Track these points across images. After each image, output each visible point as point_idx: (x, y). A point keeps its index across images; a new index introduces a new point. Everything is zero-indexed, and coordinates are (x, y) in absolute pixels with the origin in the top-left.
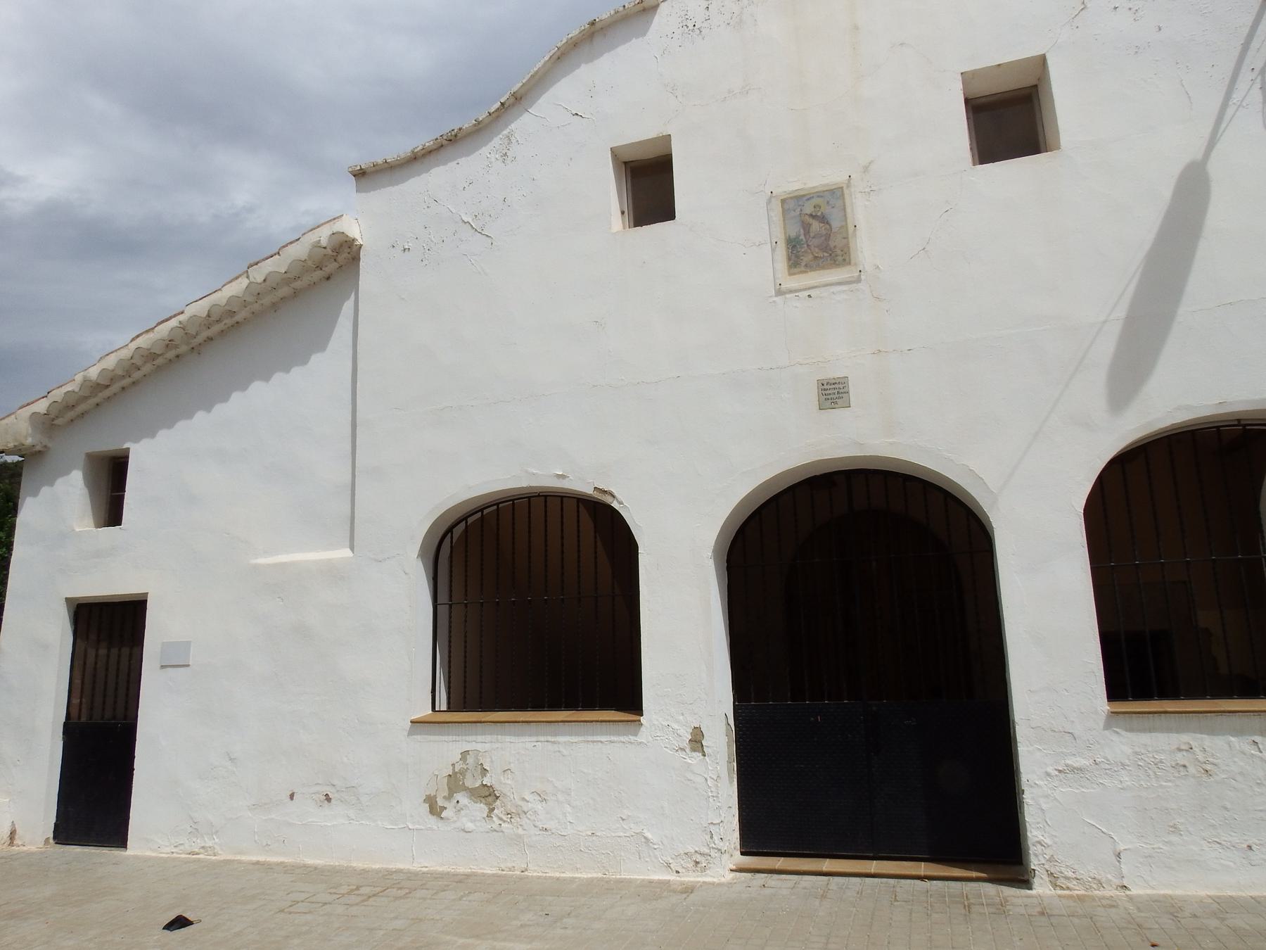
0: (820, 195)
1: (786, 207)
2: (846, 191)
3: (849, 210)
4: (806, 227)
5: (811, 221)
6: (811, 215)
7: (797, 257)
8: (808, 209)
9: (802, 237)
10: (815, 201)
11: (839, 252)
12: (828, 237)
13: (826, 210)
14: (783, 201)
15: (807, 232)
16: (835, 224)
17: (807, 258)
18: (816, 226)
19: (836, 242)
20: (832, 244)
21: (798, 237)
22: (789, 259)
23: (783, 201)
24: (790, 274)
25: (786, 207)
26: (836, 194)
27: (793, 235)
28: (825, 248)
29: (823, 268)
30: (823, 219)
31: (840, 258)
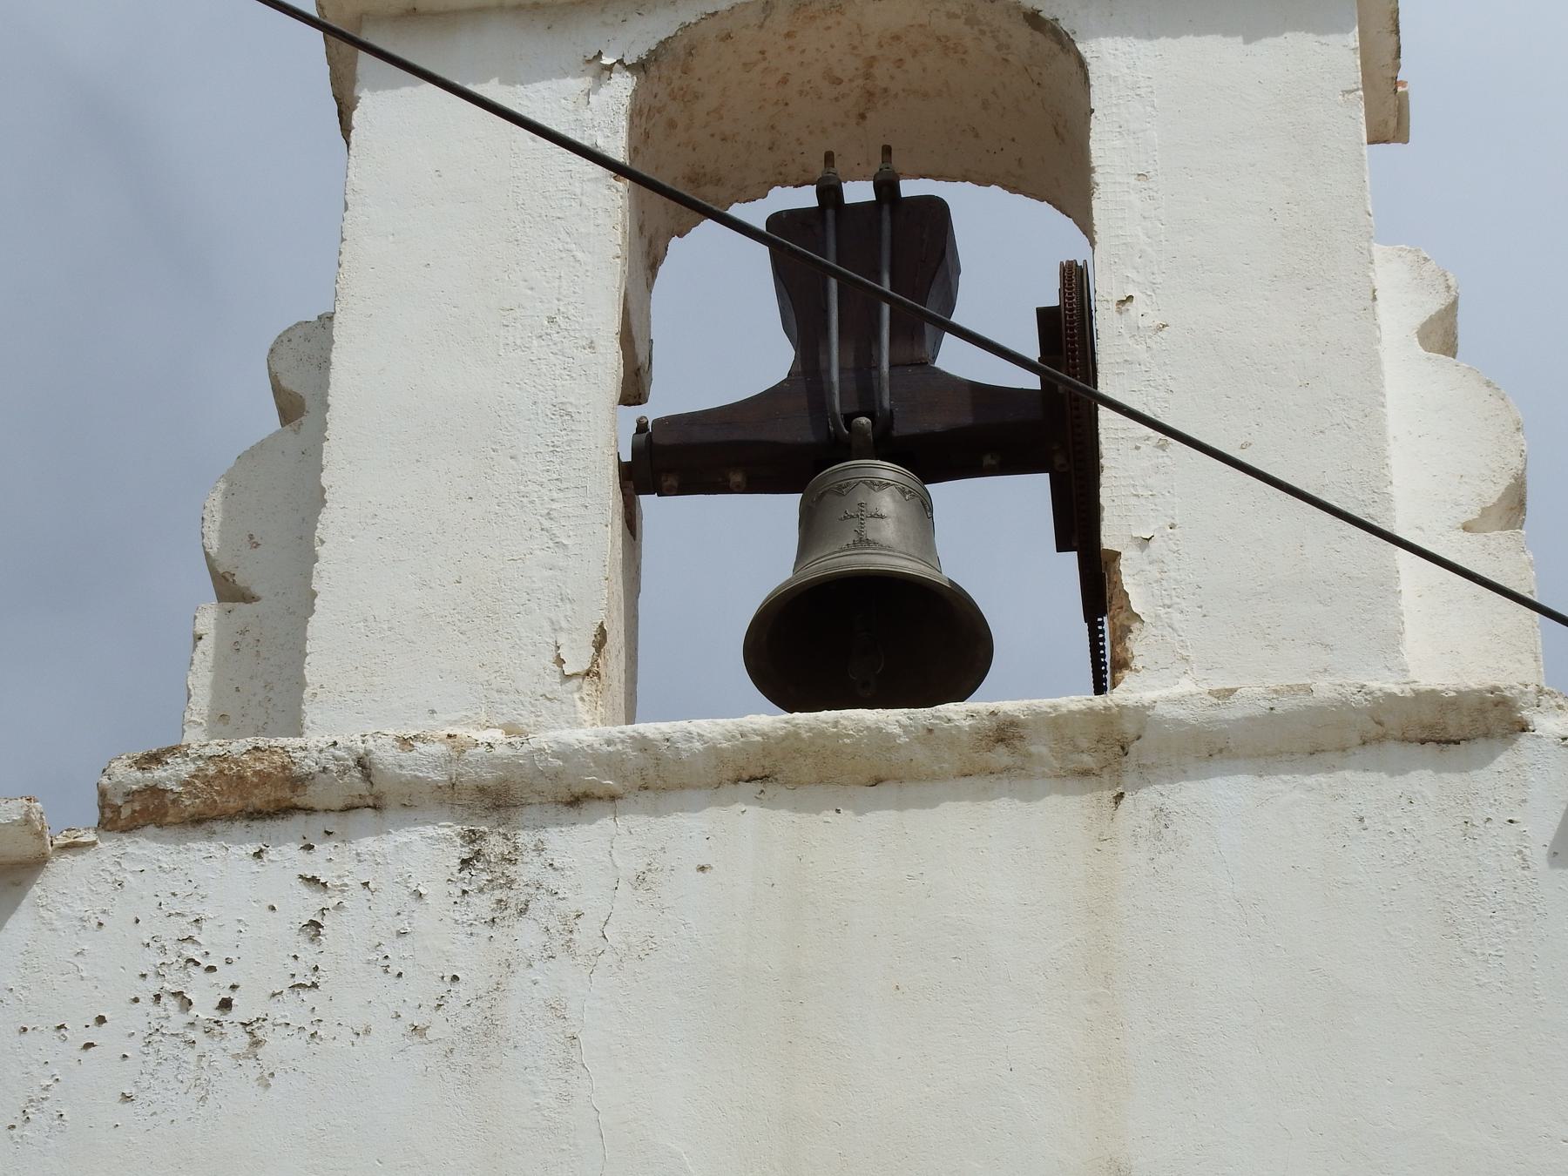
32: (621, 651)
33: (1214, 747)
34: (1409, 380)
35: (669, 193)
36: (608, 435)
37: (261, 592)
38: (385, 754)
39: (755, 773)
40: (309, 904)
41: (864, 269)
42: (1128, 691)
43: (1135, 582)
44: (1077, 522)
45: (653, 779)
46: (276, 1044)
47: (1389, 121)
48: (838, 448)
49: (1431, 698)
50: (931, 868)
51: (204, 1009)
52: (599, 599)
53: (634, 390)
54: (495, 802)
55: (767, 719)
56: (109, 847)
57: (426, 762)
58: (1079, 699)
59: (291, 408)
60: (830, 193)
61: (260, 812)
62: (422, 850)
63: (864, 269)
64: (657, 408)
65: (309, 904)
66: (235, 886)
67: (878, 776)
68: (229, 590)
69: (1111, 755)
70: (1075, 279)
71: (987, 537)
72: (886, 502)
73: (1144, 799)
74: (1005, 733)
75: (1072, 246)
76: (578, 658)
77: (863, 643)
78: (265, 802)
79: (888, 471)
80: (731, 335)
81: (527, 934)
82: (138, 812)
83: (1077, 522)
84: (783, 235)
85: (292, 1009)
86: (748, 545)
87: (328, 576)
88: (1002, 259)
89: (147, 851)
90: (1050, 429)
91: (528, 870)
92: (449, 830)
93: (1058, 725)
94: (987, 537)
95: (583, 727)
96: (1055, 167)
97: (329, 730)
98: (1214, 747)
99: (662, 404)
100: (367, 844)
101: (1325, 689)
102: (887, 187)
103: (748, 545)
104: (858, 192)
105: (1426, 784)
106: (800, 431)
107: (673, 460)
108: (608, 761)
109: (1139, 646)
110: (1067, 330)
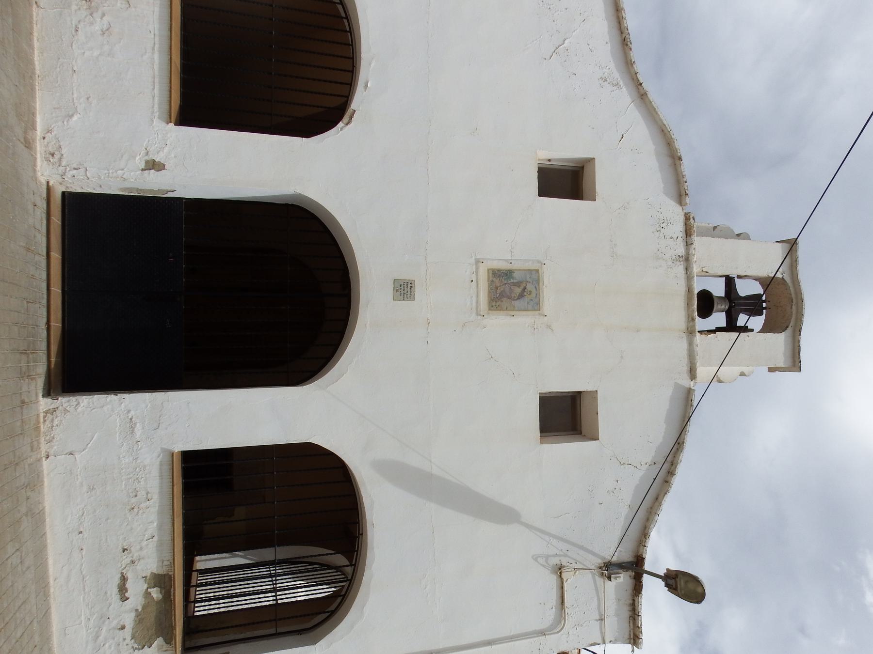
0: (538, 295)
1: (534, 273)
2: (537, 312)
3: (524, 313)
4: (518, 284)
5: (522, 287)
6: (525, 288)
7: (499, 276)
8: (530, 287)
9: (512, 281)
10: (534, 291)
11: (498, 303)
12: (509, 298)
13: (527, 298)
14: (537, 271)
15: (515, 284)
16: (517, 303)
17: (497, 282)
18: (518, 290)
19: (505, 302)
20: (504, 299)
21: (513, 278)
22: (498, 270)
23: (537, 271)
24: (488, 270)
25: (534, 273)
26: (536, 306)
27: (515, 275)
28: (503, 295)
29: (489, 292)
30: (521, 296)
31: (494, 304)
32: (705, 274)
33: (691, 344)
34: (737, 370)
35: (768, 283)
36: (733, 274)
37: (715, 231)
38: (693, 246)
39: (689, 290)
40: (675, 237)
41: (753, 306)
42: (698, 334)
43: (712, 335)
44: (719, 329)
45: (689, 278)
46: (658, 233)
47: (771, 370)
48: (730, 301)
49: (696, 370)
50: (677, 310)
51: (662, 225)
52: (712, 271)
53: (739, 277)
54: (687, 259)
55: (696, 292)
56: (683, 214)
57: (692, 251)
58: (698, 328)
59: (738, 235)
60: (764, 301)
61: (97, 632)
62: (681, 251)
63: (753, 306)
64: (736, 279)
65: (675, 237)
66: (678, 228)
67: (689, 304)
68: (715, 228)
69: (690, 332)
70: (752, 330)
71: (718, 319)
72: (723, 307)
73: (684, 335)
74: (693, 320)
75: (755, 331)
76: (704, 269)
77: (705, 303)
78: (688, 232)
79: (727, 307)
80: (745, 289)
81: (670, 263)
82: (687, 217)
83: (719, 329)
84: (760, 296)
85: (662, 235)
86: (718, 289)
87: (716, 239)
88: (757, 322)
89: (682, 218)
90: (731, 326)
91: (678, 263)
92: (683, 254)
93: (694, 326)
94: (718, 319)
95: (696, 269)
96: (765, 329)
97: (696, 239)
98: (691, 344)
99: (737, 281)
100: (52, 590)
101: (697, 357)
102: (765, 308)
103: (718, 289)
104: (764, 305)
105: (685, 368)
106: (733, 296)
107: (730, 282)
108: (691, 273)
109: (703, 336)
110: (745, 329)
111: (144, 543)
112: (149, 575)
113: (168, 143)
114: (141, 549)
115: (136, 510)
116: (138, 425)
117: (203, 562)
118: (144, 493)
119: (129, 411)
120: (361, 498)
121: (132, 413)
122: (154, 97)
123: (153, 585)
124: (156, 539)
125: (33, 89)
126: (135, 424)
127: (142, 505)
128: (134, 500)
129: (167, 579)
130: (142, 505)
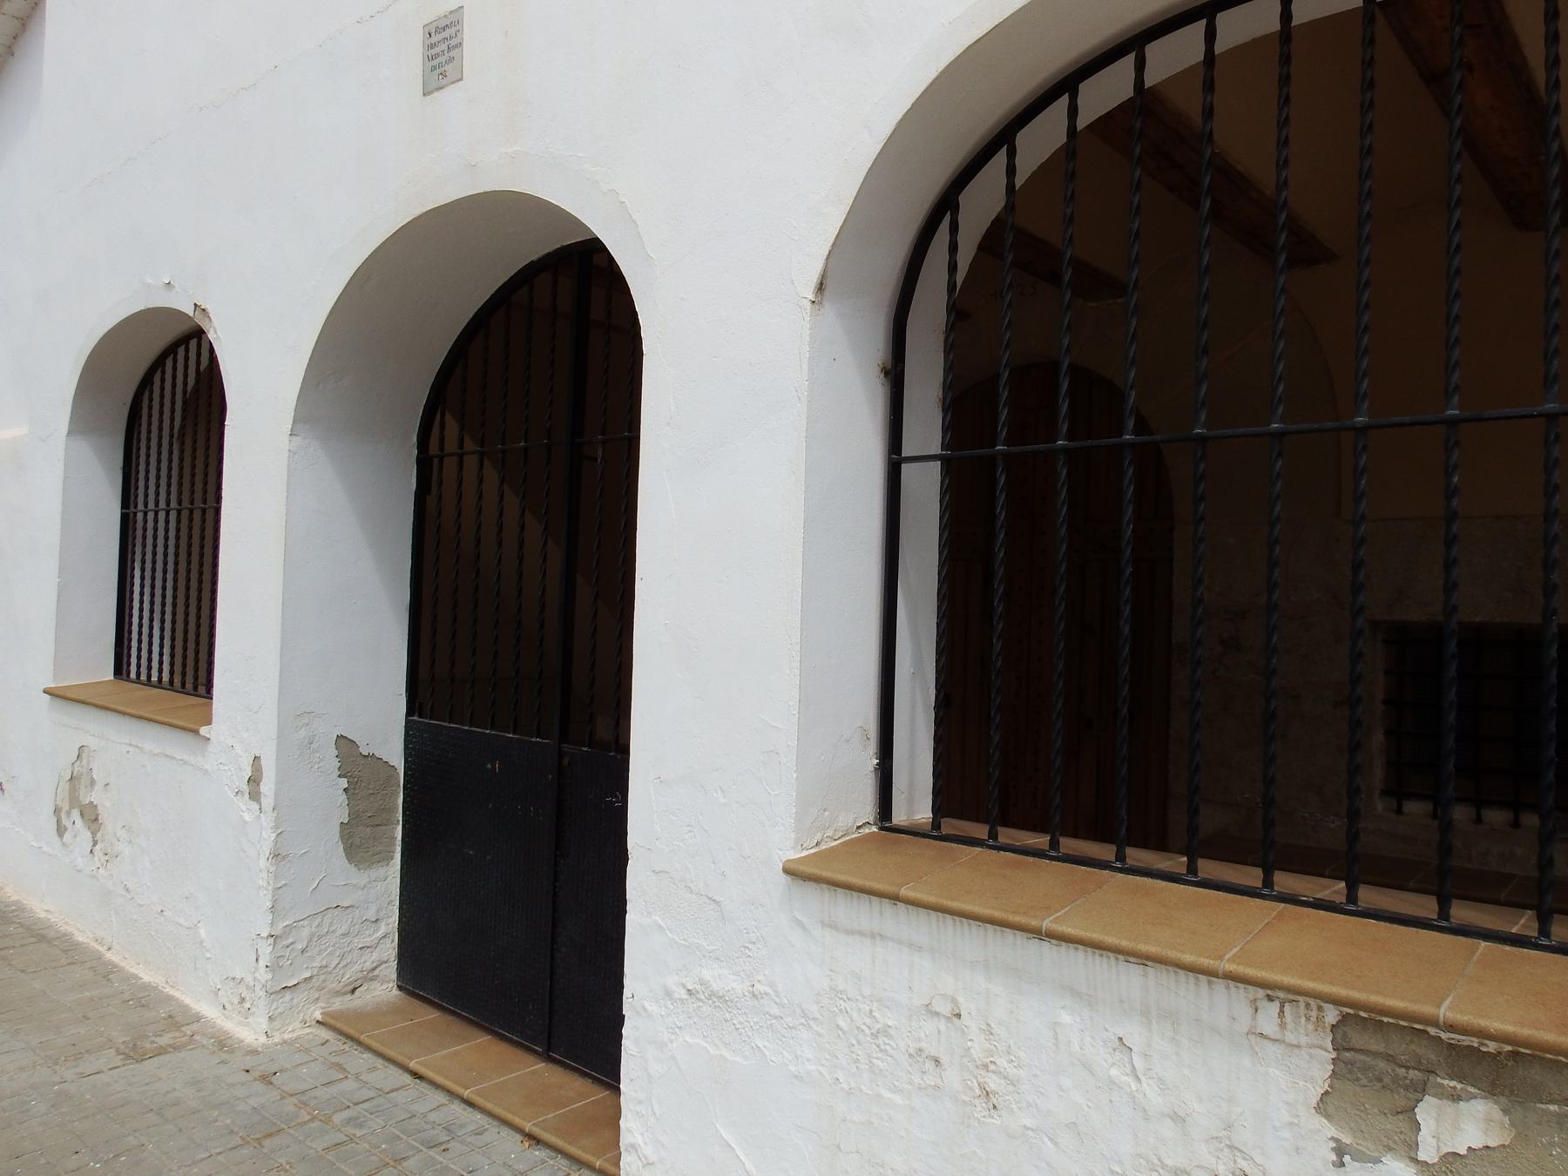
111: (1153, 1097)
112: (1331, 1131)
113: (230, 742)
114: (1178, 1119)
115: (993, 1083)
116: (706, 974)
117: (133, 675)
118: (929, 1026)
119: (668, 994)
120: (958, 49)
121: (671, 981)
122: (186, 763)
123: (1401, 1123)
124: (1133, 1032)
125: (170, 998)
126: (702, 982)
127: (978, 1049)
128: (953, 1077)
129: (1358, 1038)
130: (977, 1052)
